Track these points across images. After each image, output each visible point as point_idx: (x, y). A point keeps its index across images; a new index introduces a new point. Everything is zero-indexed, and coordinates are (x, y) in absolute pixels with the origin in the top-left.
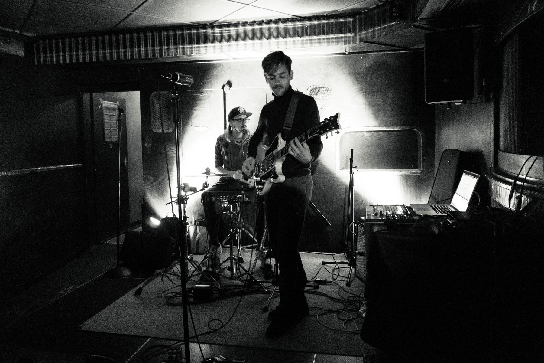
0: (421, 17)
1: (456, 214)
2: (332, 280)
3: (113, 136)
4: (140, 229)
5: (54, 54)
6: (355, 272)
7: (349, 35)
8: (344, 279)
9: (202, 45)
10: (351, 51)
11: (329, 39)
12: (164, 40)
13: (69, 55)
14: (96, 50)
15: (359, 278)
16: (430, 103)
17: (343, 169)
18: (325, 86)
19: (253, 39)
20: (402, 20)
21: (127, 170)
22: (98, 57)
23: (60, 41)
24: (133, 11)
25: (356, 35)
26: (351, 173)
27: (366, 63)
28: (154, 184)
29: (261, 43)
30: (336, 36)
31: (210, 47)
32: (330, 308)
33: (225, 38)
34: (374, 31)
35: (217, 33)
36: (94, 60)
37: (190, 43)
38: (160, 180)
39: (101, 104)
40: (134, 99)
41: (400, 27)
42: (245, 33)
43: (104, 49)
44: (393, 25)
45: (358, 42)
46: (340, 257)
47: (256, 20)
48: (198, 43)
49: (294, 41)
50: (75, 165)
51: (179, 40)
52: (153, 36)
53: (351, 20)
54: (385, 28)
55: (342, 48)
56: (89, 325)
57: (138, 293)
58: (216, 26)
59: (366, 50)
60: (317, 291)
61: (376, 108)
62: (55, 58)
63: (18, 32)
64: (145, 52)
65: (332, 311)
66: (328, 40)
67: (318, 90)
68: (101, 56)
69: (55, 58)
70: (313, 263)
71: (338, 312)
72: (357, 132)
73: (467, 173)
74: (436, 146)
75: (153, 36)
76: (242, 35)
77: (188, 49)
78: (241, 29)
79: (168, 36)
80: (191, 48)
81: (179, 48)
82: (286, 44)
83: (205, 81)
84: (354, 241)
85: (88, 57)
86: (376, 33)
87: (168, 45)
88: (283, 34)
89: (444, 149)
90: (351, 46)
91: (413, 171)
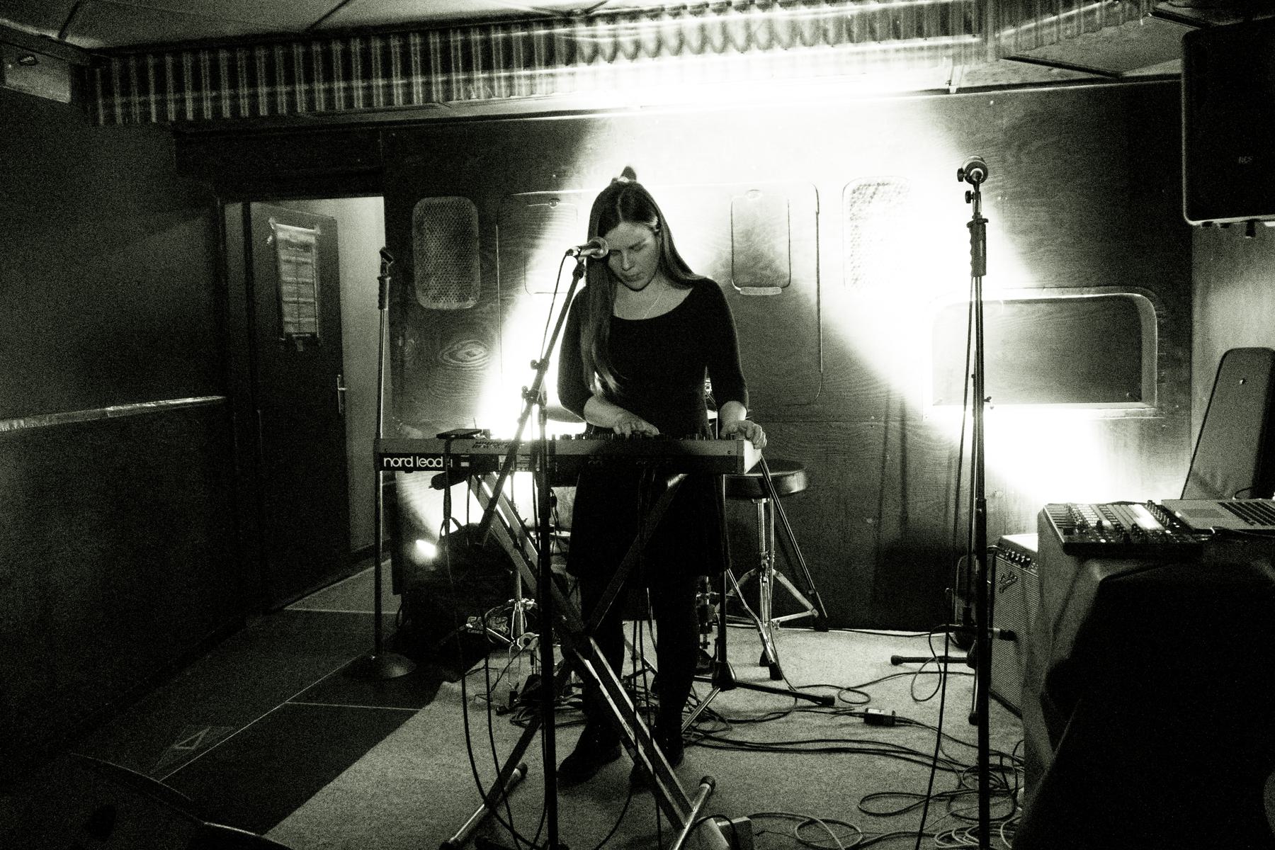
5: (152, 98)
7: (968, 39)
9: (541, 71)
10: (965, 85)
11: (911, 49)
12: (457, 55)
13: (195, 100)
14: (267, 85)
16: (1194, 223)
17: (939, 403)
21: (344, 411)
22: (272, 105)
23: (169, 60)
35: (603, 37)
37: (508, 65)
39: (274, 233)
40: (363, 220)
44: (1093, 12)
45: (990, 59)
50: (210, 398)
52: (425, 45)
54: (1070, 19)
55: (958, 74)
58: (599, 16)
59: (1004, 82)
63: (54, 35)
64: (407, 94)
66: (909, 55)
67: (872, 189)
74: (1197, 340)
75: (425, 45)
76: (673, 42)
77: (523, 81)
79: (467, 45)
80: (510, 78)
85: (244, 102)
88: (785, 37)
89: (1221, 350)
90: (967, 69)
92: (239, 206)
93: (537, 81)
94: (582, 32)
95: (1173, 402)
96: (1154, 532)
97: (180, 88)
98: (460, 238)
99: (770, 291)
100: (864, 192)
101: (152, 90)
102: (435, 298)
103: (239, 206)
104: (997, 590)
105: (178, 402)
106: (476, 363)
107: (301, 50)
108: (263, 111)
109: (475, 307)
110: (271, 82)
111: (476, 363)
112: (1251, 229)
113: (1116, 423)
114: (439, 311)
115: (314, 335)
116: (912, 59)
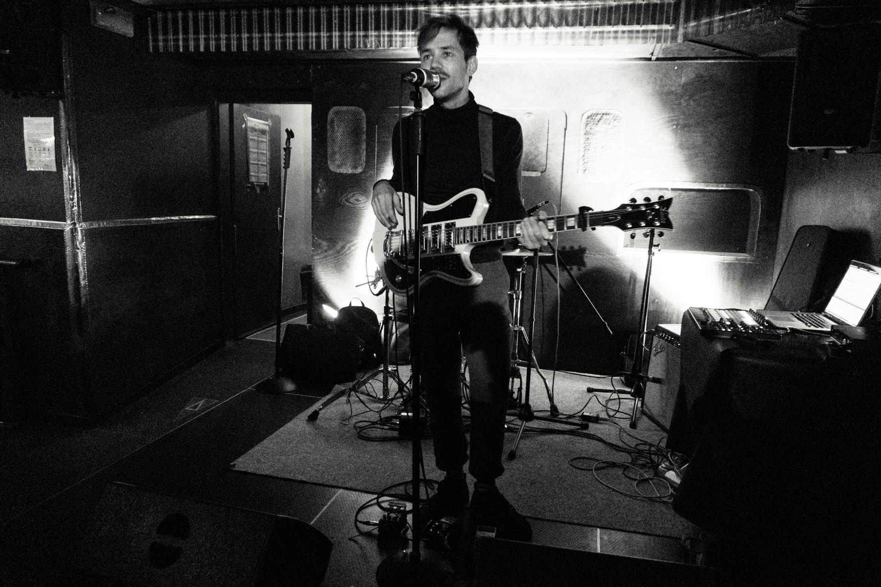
1: (840, 330)
2: (606, 417)
4: (301, 319)
5: (181, 37)
6: (642, 406)
7: (665, 27)
8: (628, 416)
10: (660, 56)
12: (359, 20)
13: (205, 39)
15: (651, 418)
16: (792, 148)
18: (611, 112)
19: (505, 25)
22: (250, 45)
23: (180, 14)
25: (677, 28)
26: (650, 252)
27: (687, 74)
28: (331, 252)
29: (519, 34)
30: (644, 27)
32: (611, 459)
33: (499, 23)
34: (710, 23)
37: (402, 28)
38: (338, 247)
39: (245, 122)
40: (298, 117)
41: (760, 17)
42: (493, 14)
44: (747, 13)
45: (680, 39)
46: (617, 383)
49: (573, 33)
51: (384, 22)
54: (732, 18)
56: (243, 463)
57: (313, 417)
60: (585, 431)
61: (691, 152)
62: (181, 43)
65: (614, 465)
66: (630, 35)
67: (599, 117)
68: (256, 42)
69: (181, 43)
70: (574, 389)
71: (625, 467)
72: (653, 189)
73: (855, 264)
75: (341, 13)
76: (489, 19)
77: (398, 39)
79: (366, 14)
81: (384, 36)
82: (560, 38)
84: (643, 362)
86: (716, 24)
87: (366, 29)
88: (556, 20)
90: (664, 46)
91: (742, 256)
92: (227, 105)
93: (406, 39)
95: (764, 255)
96: (753, 327)
97: (218, 31)
98: (355, 133)
99: (534, 174)
100: (594, 118)
101: (181, 33)
102: (339, 166)
103: (227, 105)
104: (652, 354)
105: (191, 217)
106: (361, 206)
107: (337, 10)
108: (245, 48)
109: (361, 173)
110: (250, 31)
111: (361, 206)
112: (827, 154)
113: (729, 264)
114: (340, 174)
115: (266, 184)
116: (632, 38)
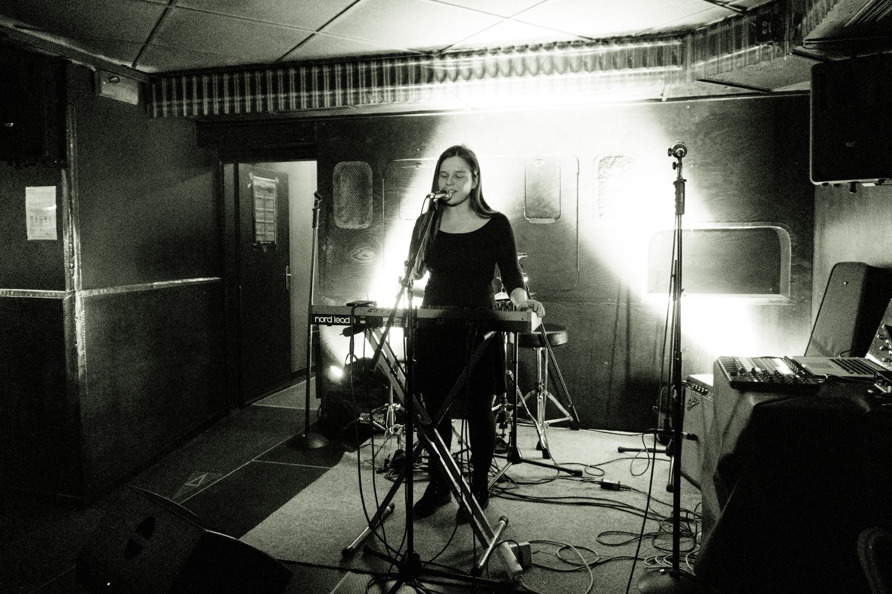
0: (807, 38)
3: (268, 233)
9: (412, 87)
10: (671, 96)
11: (639, 74)
13: (187, 105)
17: (651, 292)
20: (776, 41)
23: (194, 79)
24: (318, 31)
31: (438, 88)
36: (248, 110)
37: (393, 83)
39: (251, 182)
40: (304, 175)
43: (264, 92)
44: (754, 51)
47: (516, 45)
48: (405, 82)
50: (212, 279)
51: (387, 77)
52: (344, 71)
53: (677, 43)
54: (740, 56)
59: (696, 95)
63: (130, 65)
64: (333, 101)
67: (612, 160)
69: (185, 108)
74: (817, 256)
75: (344, 71)
78: (489, 59)
79: (368, 71)
83: (424, 144)
90: (673, 86)
91: (775, 297)
94: (437, 64)
